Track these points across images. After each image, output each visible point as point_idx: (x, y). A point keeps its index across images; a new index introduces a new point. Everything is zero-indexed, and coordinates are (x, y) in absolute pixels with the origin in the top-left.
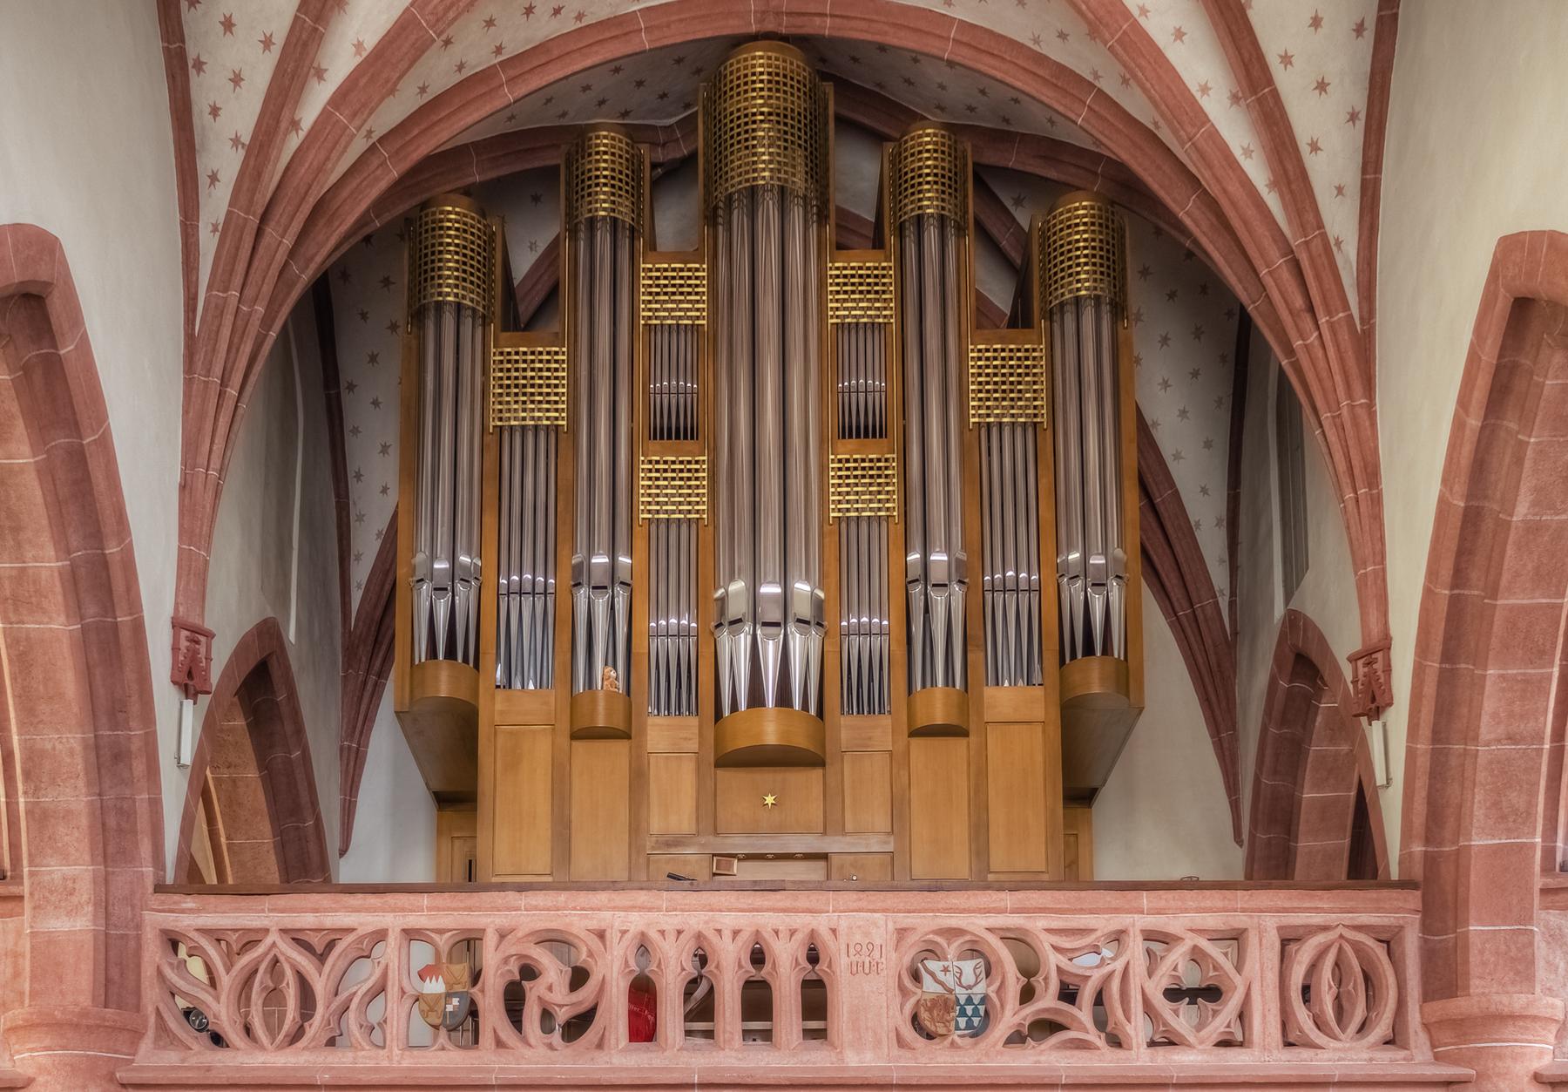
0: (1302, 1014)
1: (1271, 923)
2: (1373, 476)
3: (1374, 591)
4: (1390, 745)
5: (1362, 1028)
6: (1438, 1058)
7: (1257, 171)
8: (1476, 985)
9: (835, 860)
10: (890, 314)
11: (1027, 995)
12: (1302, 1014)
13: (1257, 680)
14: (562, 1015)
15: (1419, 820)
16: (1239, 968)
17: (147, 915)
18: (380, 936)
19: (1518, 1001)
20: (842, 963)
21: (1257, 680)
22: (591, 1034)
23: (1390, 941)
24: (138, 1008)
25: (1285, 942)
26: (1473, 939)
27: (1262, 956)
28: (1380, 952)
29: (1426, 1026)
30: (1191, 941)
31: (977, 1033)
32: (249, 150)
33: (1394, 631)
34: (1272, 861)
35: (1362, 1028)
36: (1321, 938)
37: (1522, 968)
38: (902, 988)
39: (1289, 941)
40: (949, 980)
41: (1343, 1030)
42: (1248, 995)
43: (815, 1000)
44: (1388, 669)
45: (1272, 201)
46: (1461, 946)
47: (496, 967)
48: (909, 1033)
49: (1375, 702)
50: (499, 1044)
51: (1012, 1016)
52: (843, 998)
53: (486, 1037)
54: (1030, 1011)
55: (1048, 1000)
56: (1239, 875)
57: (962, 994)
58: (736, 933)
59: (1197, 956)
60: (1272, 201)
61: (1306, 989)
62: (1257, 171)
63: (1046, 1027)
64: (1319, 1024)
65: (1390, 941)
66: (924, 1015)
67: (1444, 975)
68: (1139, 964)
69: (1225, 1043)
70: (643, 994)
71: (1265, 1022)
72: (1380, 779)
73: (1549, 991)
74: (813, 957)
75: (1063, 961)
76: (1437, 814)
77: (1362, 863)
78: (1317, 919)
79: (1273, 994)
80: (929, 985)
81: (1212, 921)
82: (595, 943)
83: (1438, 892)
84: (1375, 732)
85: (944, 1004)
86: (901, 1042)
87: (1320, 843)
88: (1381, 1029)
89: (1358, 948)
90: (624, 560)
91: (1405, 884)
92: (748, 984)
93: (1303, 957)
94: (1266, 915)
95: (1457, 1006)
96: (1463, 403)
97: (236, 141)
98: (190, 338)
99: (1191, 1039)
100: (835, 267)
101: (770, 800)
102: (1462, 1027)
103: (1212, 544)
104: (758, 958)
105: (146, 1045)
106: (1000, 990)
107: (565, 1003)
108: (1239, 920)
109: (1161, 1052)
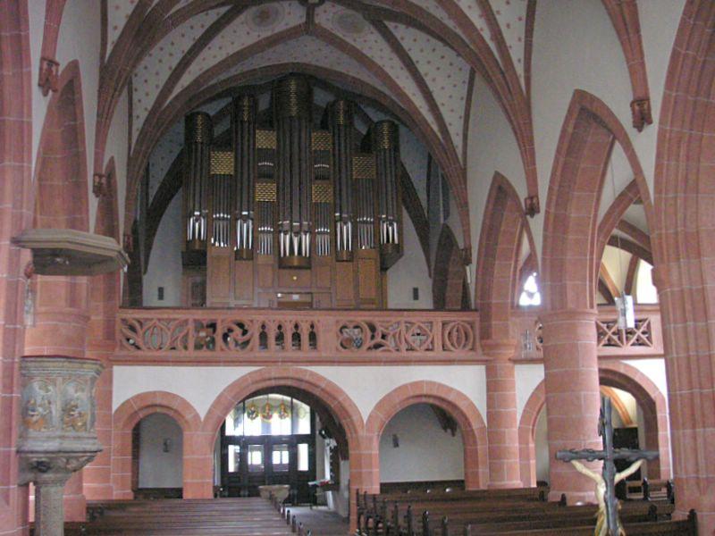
0: (448, 342)
1: (440, 319)
2: (466, 203)
3: (467, 233)
4: (471, 272)
5: (464, 346)
6: (484, 354)
7: (435, 128)
8: (494, 337)
9: (314, 295)
10: (330, 148)
11: (373, 337)
12: (448, 342)
13: (434, 242)
14: (240, 342)
15: (479, 294)
16: (431, 331)
17: (118, 314)
18: (186, 321)
19: (505, 341)
20: (321, 329)
21: (434, 242)
22: (249, 347)
23: (472, 325)
24: (114, 339)
25: (443, 324)
26: (493, 326)
27: (437, 328)
28: (468, 327)
29: (481, 346)
30: (418, 324)
31: (359, 347)
32: (150, 113)
33: (473, 245)
34: (440, 304)
35: (464, 346)
36: (453, 324)
37: (506, 333)
38: (337, 336)
39: (444, 324)
40: (351, 334)
41: (459, 346)
42: (433, 339)
43: (313, 337)
44: (471, 254)
45: (439, 134)
46: (489, 326)
47: (220, 330)
48: (340, 348)
49: (468, 261)
50: (222, 350)
51: (370, 343)
52: (322, 339)
53: (218, 348)
54: (373, 342)
55: (378, 339)
56: (431, 307)
57: (355, 337)
58: (291, 321)
59: (420, 327)
60: (439, 134)
61: (450, 333)
62: (435, 128)
63: (377, 346)
64: (452, 345)
65: (472, 325)
66: (344, 343)
67: (486, 334)
68: (404, 328)
69: (427, 350)
70: (263, 336)
71: (438, 344)
72: (469, 281)
73: (513, 338)
74: (312, 326)
75: (382, 329)
76: (484, 292)
77: (465, 306)
78: (452, 319)
79: (440, 337)
80: (345, 335)
81: (424, 319)
82: (249, 323)
83: (485, 312)
84: (468, 268)
85: (350, 340)
86: (337, 349)
87: (453, 294)
88: (470, 346)
89: (463, 326)
90: (251, 212)
91: (476, 310)
92: (293, 334)
93: (448, 329)
94: (439, 318)
95: (489, 342)
96: (488, 201)
97: (146, 109)
98: (129, 158)
99: (418, 349)
100: (313, 134)
101: (295, 278)
102: (492, 347)
103: (422, 196)
104: (296, 326)
105: (117, 349)
106: (365, 336)
107: (241, 339)
108: (432, 319)
109: (410, 352)
